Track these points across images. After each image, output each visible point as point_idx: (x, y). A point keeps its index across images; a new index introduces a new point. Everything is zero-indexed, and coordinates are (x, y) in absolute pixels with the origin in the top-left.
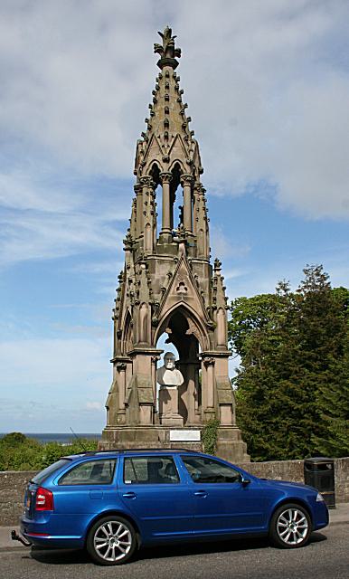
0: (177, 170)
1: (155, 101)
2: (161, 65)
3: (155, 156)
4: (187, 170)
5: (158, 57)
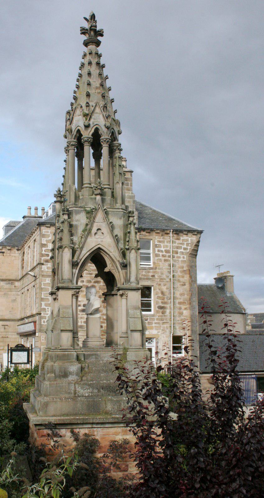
0: (96, 135)
1: (78, 87)
2: (86, 44)
3: (79, 122)
4: (105, 135)
5: (85, 38)
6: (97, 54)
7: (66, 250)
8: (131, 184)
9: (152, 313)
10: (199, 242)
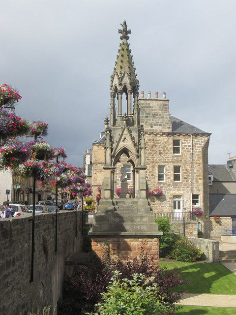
2: (121, 39)
5: (121, 35)
6: (127, 44)
7: (108, 149)
8: (168, 108)
9: (181, 181)
10: (209, 140)
